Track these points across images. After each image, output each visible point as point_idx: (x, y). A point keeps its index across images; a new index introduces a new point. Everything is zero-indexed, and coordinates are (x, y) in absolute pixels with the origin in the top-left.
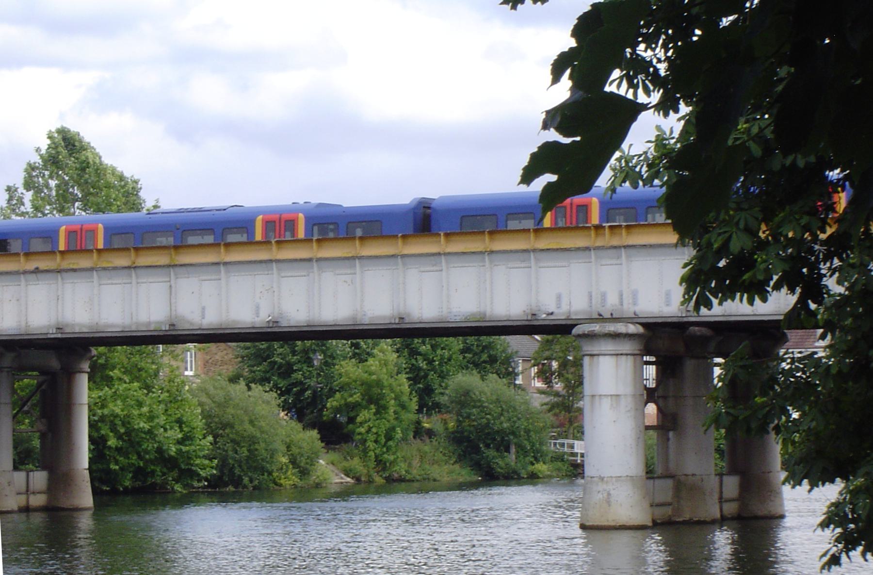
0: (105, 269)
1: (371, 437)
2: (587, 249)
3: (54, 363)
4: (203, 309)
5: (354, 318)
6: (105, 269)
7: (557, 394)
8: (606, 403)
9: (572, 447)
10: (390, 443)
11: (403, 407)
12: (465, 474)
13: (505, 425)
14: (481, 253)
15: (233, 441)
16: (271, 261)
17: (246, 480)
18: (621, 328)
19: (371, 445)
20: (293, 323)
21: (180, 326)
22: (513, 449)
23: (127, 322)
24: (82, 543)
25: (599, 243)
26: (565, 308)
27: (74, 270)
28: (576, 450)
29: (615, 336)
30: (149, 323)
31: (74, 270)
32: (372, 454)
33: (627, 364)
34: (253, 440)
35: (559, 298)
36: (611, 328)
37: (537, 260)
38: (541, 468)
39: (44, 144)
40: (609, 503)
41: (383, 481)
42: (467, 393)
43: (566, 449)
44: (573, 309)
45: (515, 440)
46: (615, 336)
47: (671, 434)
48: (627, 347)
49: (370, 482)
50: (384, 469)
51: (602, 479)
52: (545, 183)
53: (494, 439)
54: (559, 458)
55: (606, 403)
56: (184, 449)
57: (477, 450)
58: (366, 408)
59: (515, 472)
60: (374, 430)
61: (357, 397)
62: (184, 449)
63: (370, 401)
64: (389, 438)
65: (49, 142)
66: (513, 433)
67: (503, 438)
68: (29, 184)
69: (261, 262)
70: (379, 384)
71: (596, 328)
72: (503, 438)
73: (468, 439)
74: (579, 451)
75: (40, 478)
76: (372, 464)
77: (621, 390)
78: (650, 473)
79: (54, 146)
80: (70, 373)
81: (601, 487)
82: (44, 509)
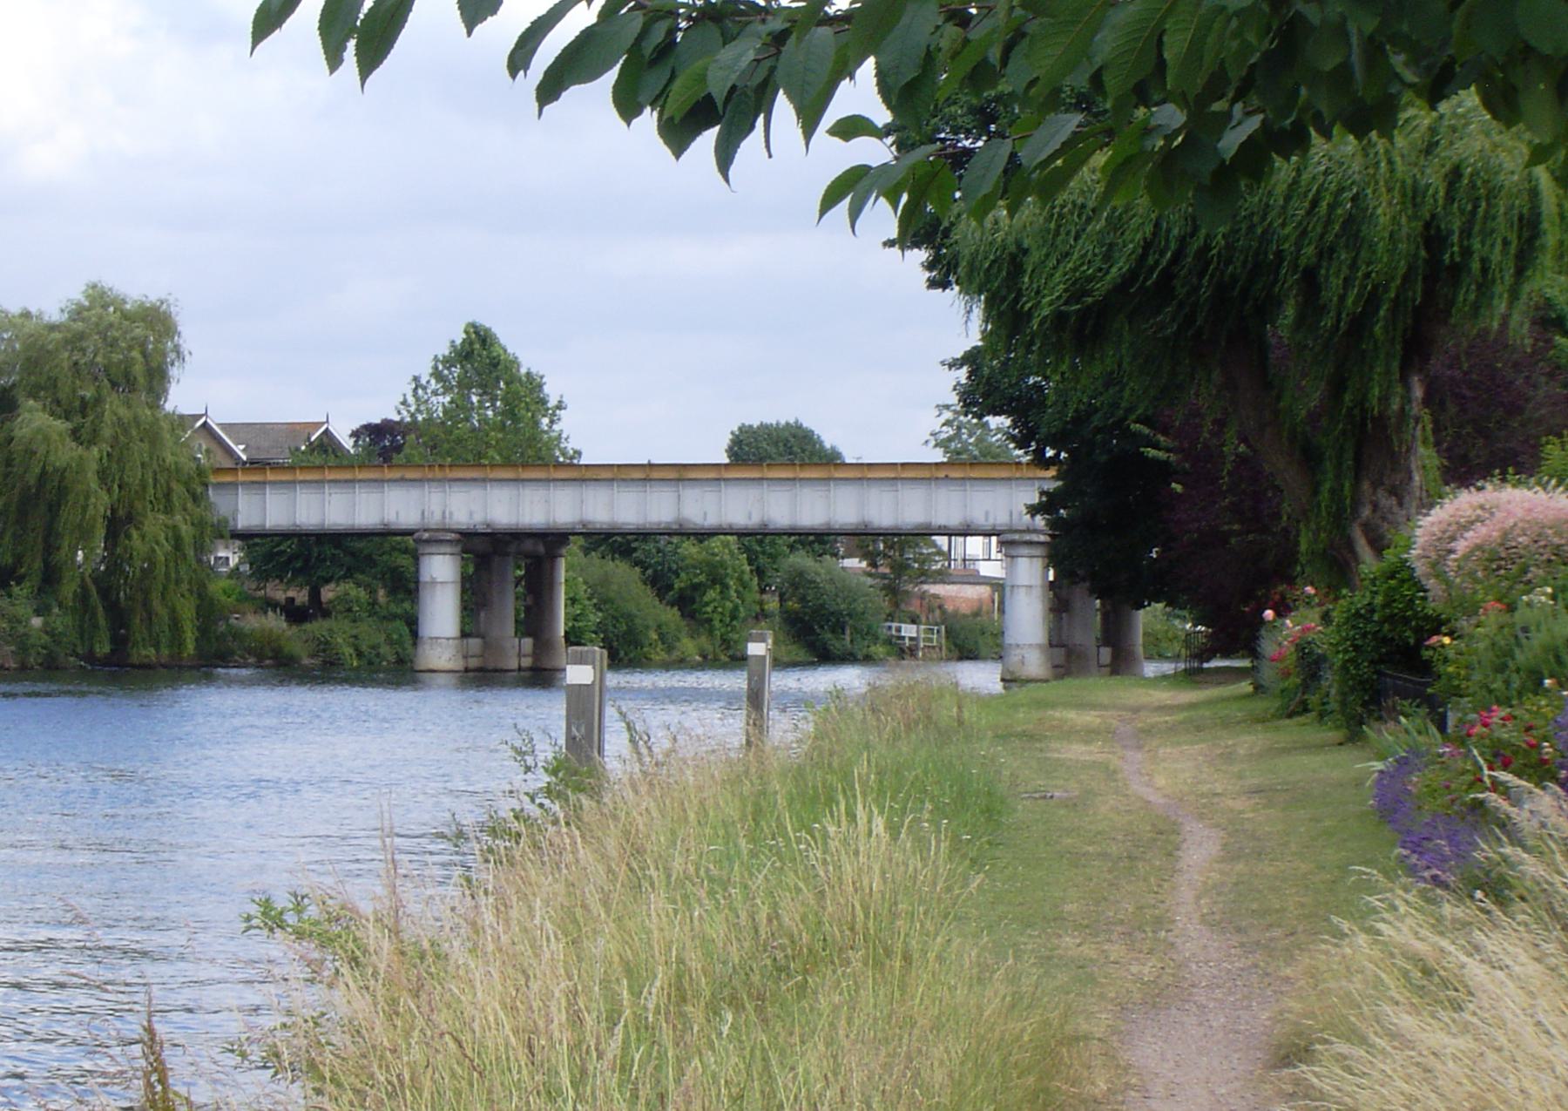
0: (623, 480)
1: (717, 617)
2: (1009, 479)
3: (541, 549)
4: (705, 514)
5: (828, 524)
6: (623, 480)
7: (884, 576)
8: (1022, 591)
9: (899, 630)
10: (734, 623)
11: (745, 586)
12: (802, 655)
13: (842, 606)
14: (929, 479)
15: (614, 617)
16: (762, 479)
17: (622, 653)
18: (1035, 538)
19: (717, 623)
20: (778, 526)
21: (686, 526)
22: (848, 632)
23: (641, 521)
24: (1450, 563)
25: (1018, 475)
26: (991, 521)
27: (596, 480)
28: (903, 634)
29: (1030, 543)
30: (659, 524)
31: (596, 480)
32: (718, 633)
33: (1038, 564)
34: (630, 617)
35: (987, 513)
36: (1027, 537)
37: (972, 486)
38: (879, 650)
39: (459, 337)
40: (1023, 663)
41: (727, 659)
42: (801, 574)
43: (894, 632)
44: (998, 522)
45: (851, 622)
46: (1030, 543)
47: (1064, 615)
48: (1038, 551)
49: (716, 659)
50: (728, 648)
51: (1018, 646)
52: (499, 12)
53: (829, 620)
54: (889, 642)
55: (1022, 591)
56: (577, 624)
57: (811, 631)
58: (711, 587)
59: (851, 654)
60: (720, 610)
61: (702, 578)
62: (577, 624)
63: (714, 582)
64: (734, 617)
65: (464, 336)
66: (850, 615)
67: (838, 620)
68: (437, 374)
69: (754, 479)
70: (722, 564)
71: (1017, 537)
72: (838, 620)
73: (802, 621)
74: (907, 635)
75: (528, 643)
76: (718, 642)
77: (1033, 582)
78: (1051, 645)
79: (468, 342)
80: (553, 557)
81: (1018, 651)
82: (531, 669)
